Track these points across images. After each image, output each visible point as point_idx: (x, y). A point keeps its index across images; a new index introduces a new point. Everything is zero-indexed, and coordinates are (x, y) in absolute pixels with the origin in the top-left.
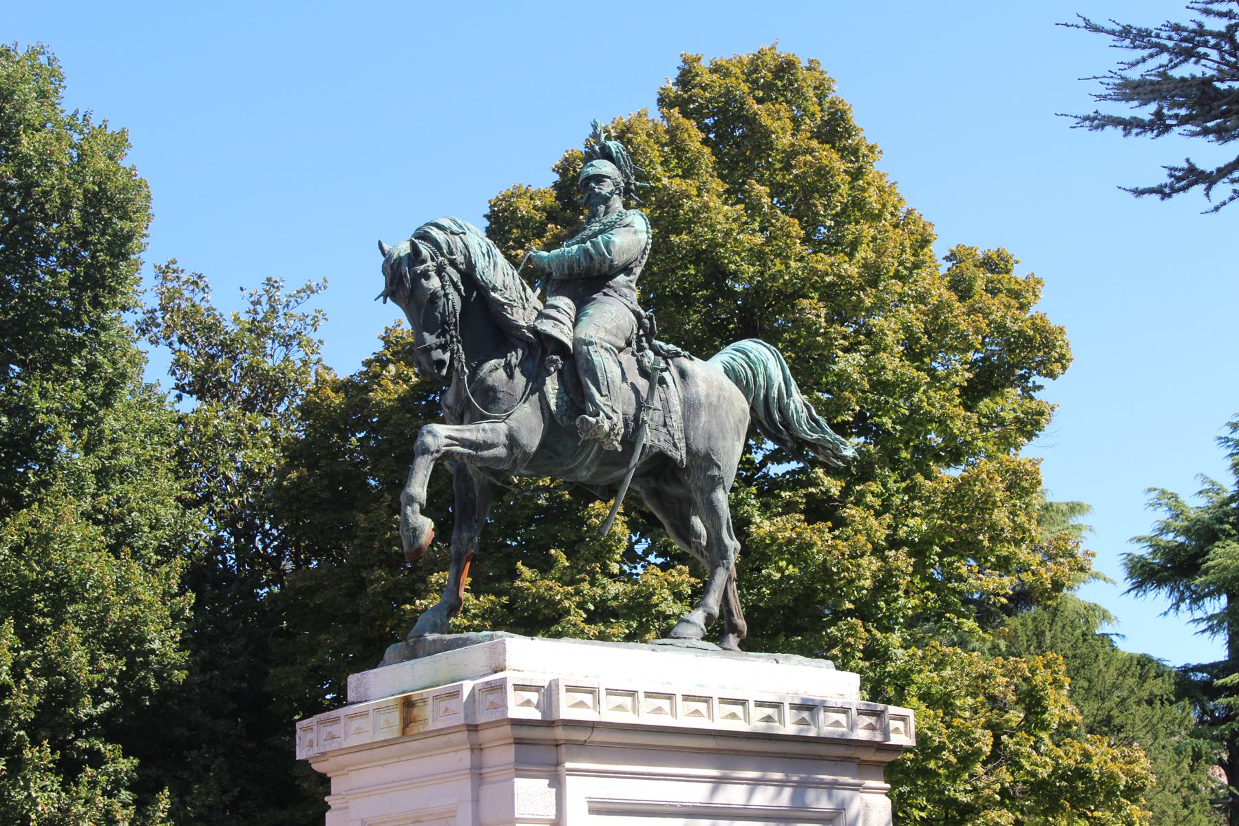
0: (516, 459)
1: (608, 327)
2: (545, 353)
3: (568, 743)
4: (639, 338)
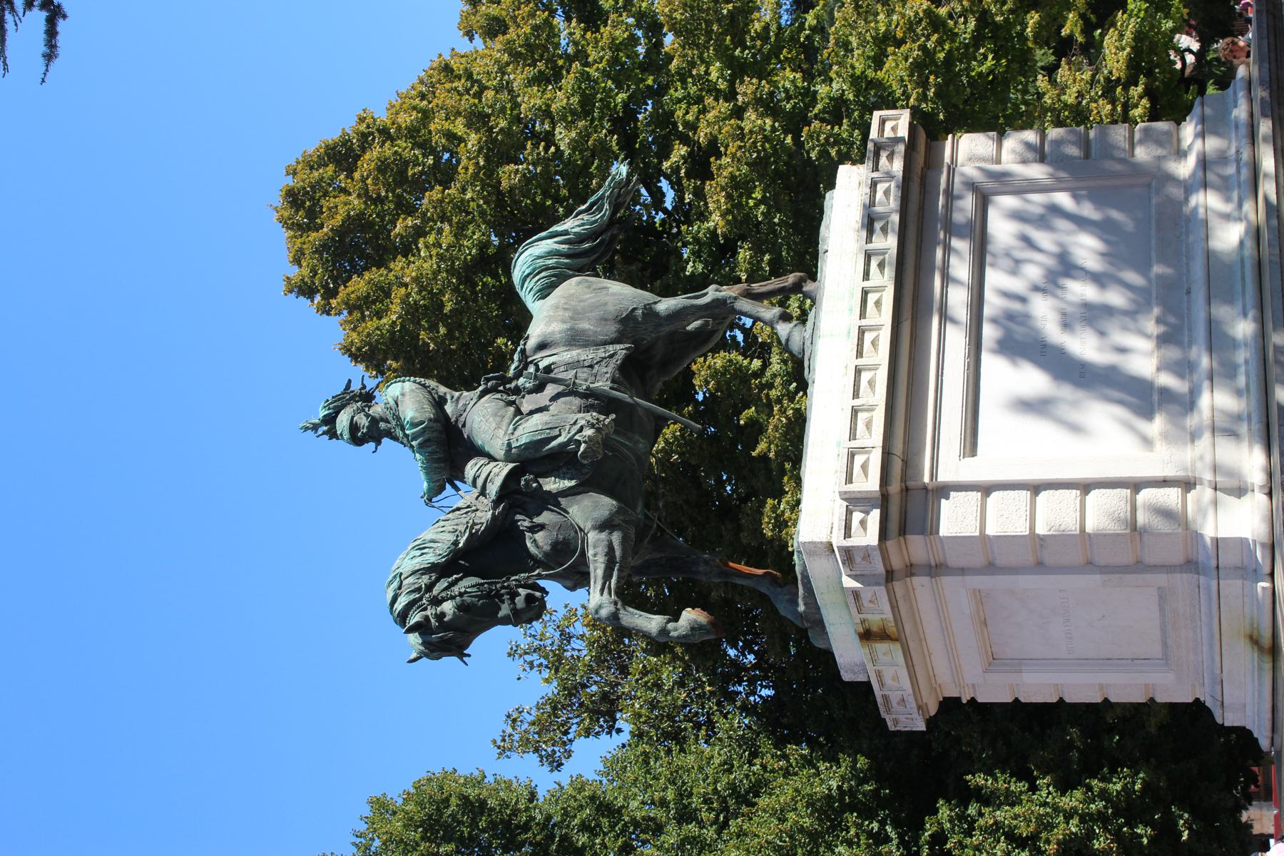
0: (624, 521)
1: (494, 425)
2: (518, 491)
3: (904, 478)
4: (507, 392)
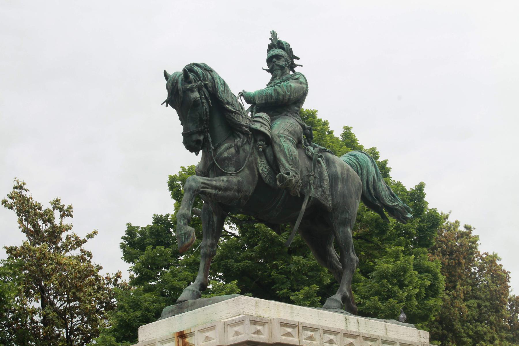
1: (290, 130)
